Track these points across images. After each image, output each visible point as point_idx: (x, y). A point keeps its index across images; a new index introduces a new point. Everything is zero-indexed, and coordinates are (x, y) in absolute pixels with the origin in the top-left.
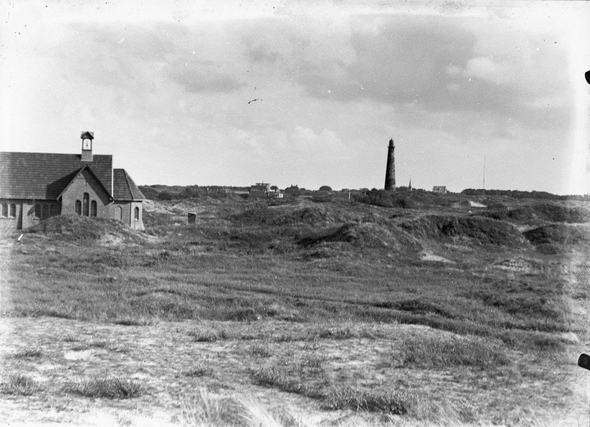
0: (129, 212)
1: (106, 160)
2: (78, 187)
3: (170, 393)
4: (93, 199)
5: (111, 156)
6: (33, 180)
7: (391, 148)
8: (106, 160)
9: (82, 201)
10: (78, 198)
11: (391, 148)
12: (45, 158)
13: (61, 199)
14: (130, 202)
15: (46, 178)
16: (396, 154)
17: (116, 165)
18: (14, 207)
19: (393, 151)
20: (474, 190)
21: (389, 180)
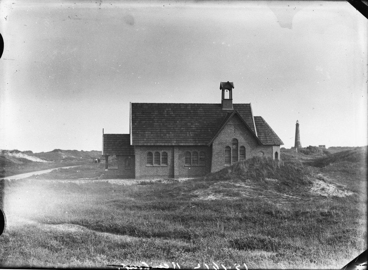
0: (271, 151)
1: (247, 107)
2: (229, 134)
3: (329, 244)
4: (241, 145)
5: (249, 104)
6: (182, 129)
7: (297, 125)
8: (247, 107)
9: (231, 146)
10: (227, 144)
11: (297, 125)
12: (196, 105)
13: (212, 145)
14: (272, 146)
15: (194, 126)
16: (300, 128)
17: (255, 113)
18: (158, 154)
19: (298, 127)
20: (335, 147)
21: (297, 143)
